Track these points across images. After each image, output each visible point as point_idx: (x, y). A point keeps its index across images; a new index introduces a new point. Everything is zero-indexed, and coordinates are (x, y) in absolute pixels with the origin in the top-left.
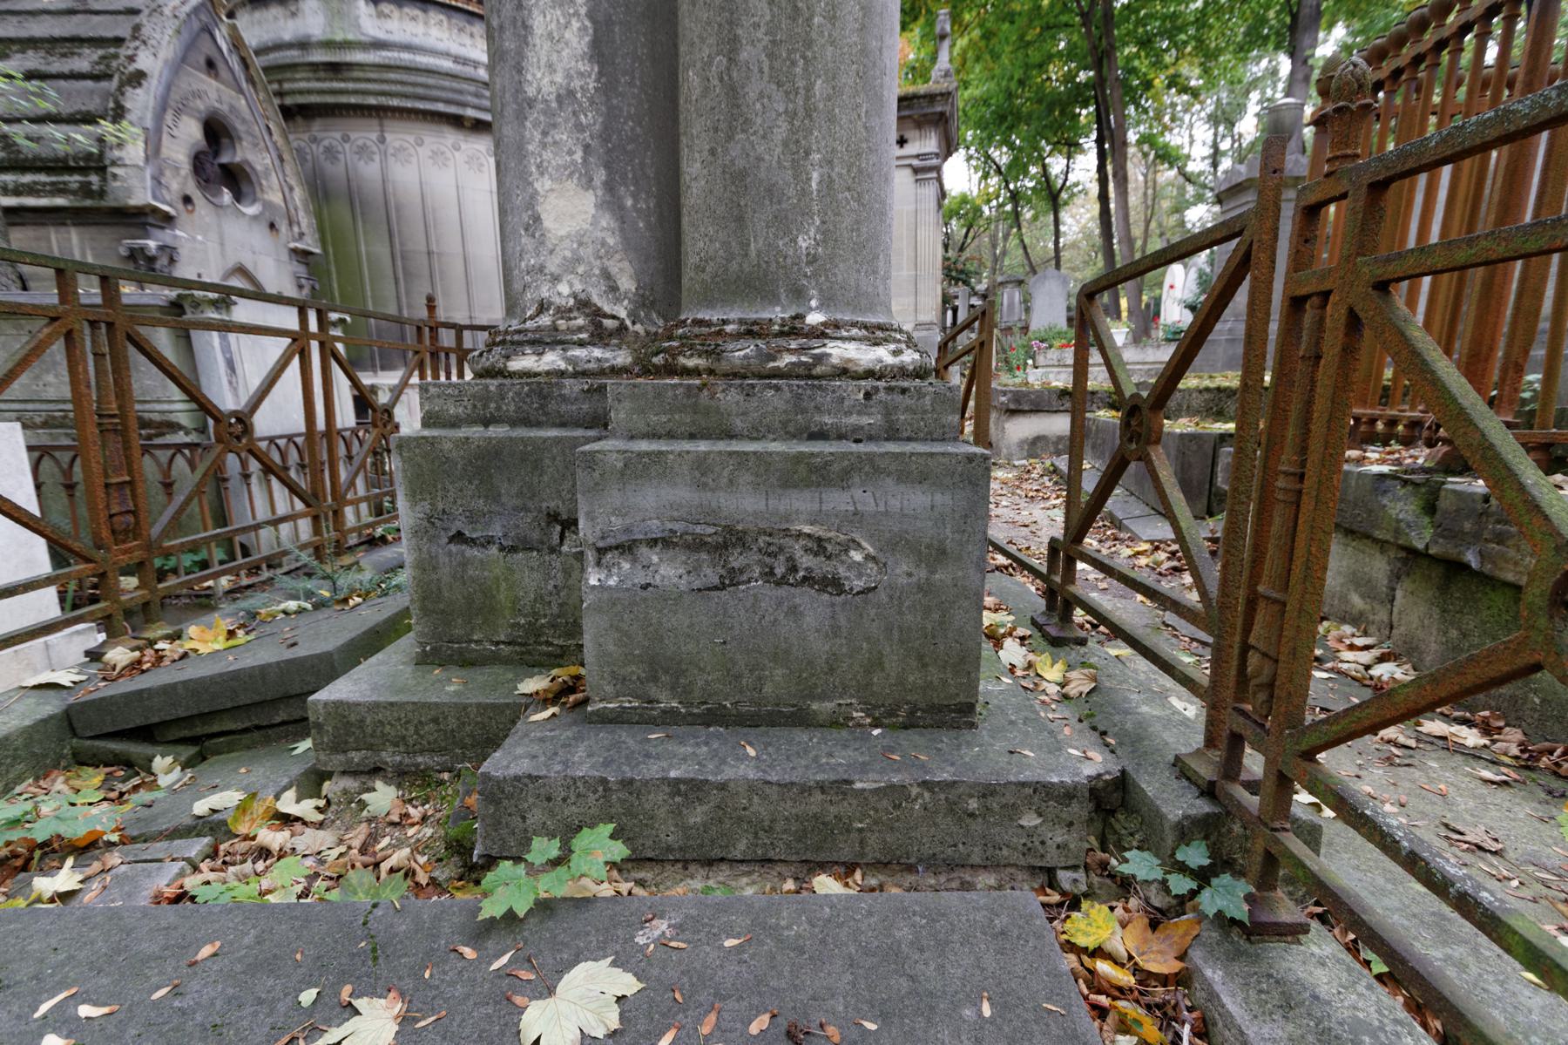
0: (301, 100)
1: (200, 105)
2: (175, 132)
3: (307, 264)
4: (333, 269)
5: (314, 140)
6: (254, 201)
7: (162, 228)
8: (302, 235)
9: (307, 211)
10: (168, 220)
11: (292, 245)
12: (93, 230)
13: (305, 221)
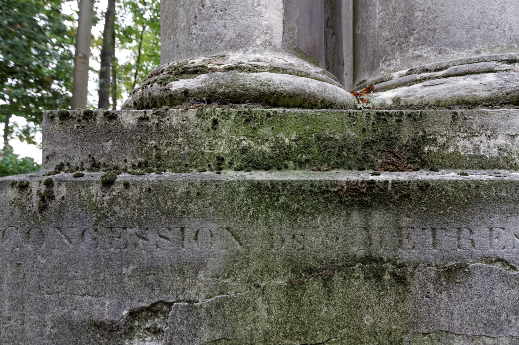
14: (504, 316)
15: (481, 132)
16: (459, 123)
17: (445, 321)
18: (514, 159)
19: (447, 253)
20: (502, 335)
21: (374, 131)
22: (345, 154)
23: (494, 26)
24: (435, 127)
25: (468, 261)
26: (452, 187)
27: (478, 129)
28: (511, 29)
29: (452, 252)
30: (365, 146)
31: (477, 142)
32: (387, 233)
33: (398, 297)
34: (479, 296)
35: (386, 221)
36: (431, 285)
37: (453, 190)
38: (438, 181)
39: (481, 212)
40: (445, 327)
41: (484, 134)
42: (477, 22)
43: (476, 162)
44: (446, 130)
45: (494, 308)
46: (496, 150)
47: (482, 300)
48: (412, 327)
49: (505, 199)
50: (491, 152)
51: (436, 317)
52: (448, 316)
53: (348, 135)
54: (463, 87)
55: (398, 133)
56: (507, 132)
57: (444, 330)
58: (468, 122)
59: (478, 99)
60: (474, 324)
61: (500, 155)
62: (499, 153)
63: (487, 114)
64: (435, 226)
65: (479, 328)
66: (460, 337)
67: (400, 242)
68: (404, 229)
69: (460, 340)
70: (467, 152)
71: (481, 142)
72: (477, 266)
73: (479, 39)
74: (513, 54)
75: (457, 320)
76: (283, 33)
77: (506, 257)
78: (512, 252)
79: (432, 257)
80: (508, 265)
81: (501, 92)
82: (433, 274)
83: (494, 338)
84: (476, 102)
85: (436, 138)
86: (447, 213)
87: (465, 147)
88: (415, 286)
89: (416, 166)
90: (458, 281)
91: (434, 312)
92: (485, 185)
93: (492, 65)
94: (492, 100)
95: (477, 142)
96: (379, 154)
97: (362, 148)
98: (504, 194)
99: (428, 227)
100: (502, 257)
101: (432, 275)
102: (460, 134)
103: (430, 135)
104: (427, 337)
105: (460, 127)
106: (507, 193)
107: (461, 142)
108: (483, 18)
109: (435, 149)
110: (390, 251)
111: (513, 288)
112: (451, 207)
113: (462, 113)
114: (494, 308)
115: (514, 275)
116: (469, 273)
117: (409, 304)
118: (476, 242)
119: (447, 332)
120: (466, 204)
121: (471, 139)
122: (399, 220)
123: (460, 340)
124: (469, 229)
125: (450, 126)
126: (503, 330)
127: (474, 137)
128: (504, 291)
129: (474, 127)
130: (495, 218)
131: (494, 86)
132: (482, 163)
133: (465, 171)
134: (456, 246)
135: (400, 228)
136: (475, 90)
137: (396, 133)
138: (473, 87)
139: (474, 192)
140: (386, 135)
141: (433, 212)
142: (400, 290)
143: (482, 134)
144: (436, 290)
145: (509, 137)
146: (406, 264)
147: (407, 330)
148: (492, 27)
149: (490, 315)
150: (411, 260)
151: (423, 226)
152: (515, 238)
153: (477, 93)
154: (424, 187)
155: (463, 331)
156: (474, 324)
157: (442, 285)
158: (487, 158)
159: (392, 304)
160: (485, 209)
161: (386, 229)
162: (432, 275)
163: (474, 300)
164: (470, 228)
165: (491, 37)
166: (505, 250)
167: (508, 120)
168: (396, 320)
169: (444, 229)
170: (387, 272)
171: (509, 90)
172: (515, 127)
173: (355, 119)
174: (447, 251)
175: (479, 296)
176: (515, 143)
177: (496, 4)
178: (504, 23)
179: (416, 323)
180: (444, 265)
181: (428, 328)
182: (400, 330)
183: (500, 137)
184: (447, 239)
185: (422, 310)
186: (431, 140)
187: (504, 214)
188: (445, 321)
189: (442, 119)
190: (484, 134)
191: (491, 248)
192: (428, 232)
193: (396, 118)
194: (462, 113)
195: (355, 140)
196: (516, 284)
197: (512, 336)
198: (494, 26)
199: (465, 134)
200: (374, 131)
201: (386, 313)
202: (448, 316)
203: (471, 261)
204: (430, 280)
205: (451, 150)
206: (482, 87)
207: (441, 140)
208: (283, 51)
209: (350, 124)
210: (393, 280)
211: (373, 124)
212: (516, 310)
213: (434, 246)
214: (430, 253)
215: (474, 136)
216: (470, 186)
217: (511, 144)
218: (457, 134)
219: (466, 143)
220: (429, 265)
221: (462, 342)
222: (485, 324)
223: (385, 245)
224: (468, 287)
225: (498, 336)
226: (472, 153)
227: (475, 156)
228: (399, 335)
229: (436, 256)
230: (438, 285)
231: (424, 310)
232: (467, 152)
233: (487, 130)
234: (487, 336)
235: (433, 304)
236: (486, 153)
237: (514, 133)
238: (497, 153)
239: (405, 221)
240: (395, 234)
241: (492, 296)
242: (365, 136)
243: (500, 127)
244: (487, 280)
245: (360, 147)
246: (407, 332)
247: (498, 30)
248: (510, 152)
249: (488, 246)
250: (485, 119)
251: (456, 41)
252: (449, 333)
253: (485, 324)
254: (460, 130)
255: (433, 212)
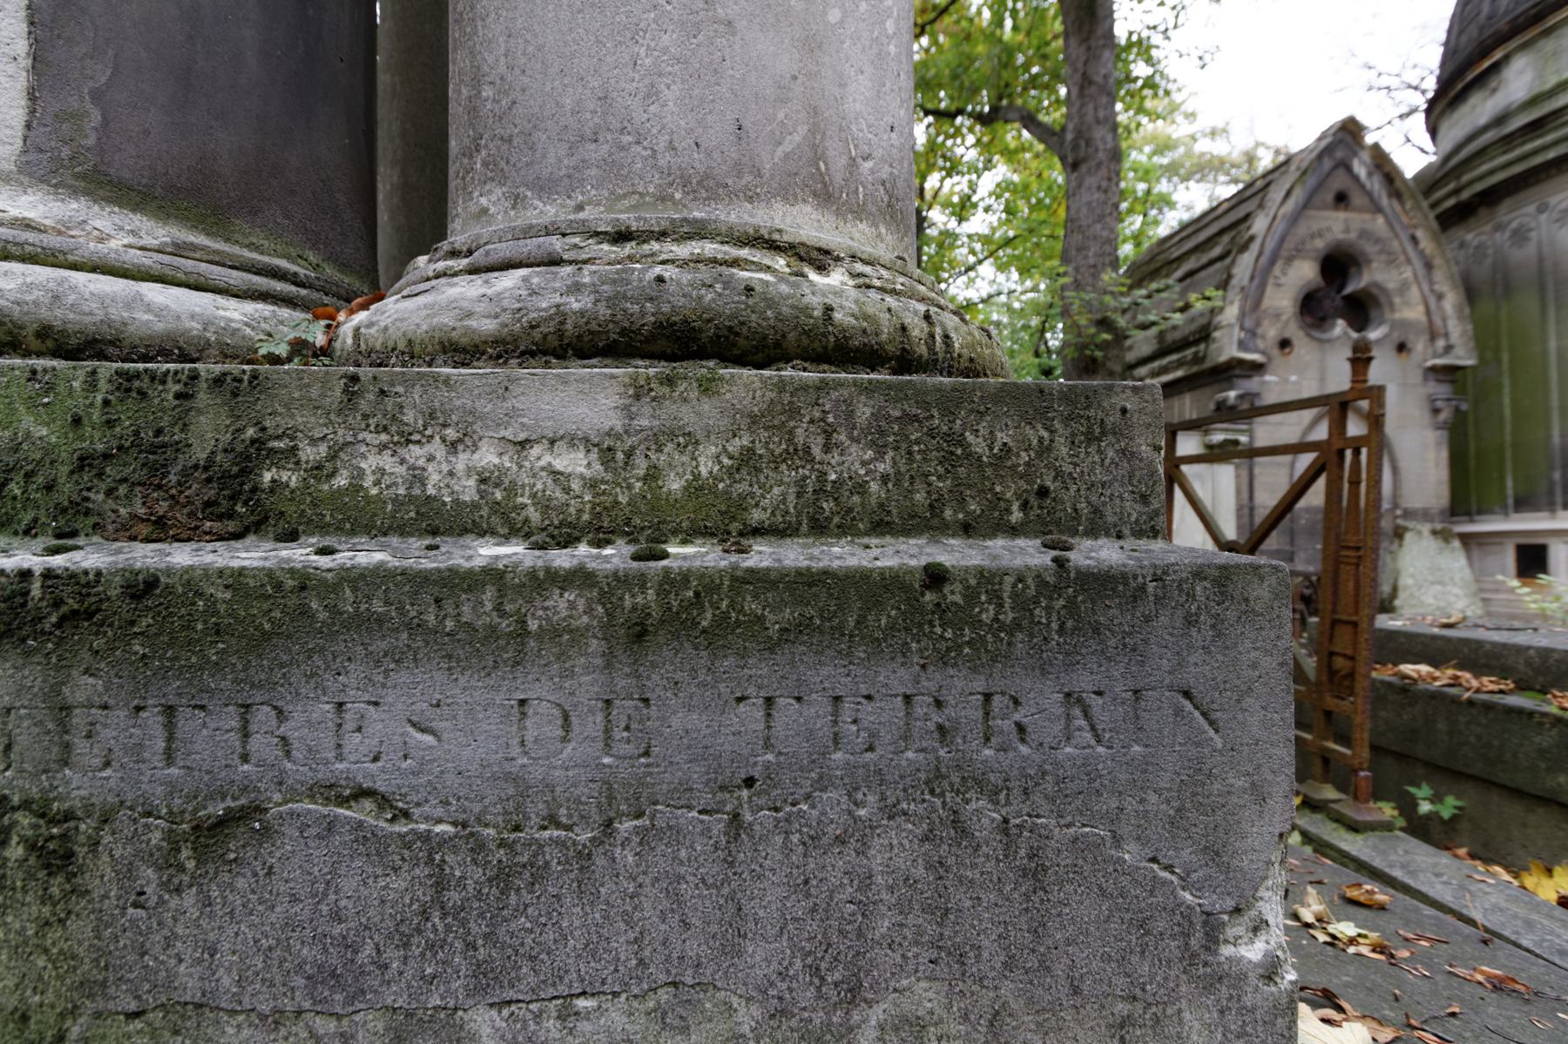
0: (1479, 187)
1: (1320, 244)
2: (1283, 280)
3: (1453, 382)
4: (1506, 381)
5: (1500, 227)
6: (1380, 324)
7: (1249, 377)
8: (1449, 349)
9: (1461, 318)
10: (1257, 368)
11: (1429, 363)
12: (1198, 392)
13: (1457, 330)
14: (369, 950)
15: (428, 432)
16: (363, 405)
17: (191, 975)
18: (524, 506)
19: (206, 778)
20: (362, 1006)
21: (110, 424)
22: (18, 492)
23: (630, 139)
24: (292, 416)
25: (269, 800)
26: (227, 587)
27: (420, 422)
28: (671, 147)
29: (223, 774)
30: (81, 468)
31: (417, 458)
32: (25, 724)
33: (46, 910)
34: (294, 899)
35: (20, 690)
36: (149, 871)
37: (228, 595)
38: (187, 572)
39: (310, 657)
40: (192, 992)
41: (437, 438)
42: (591, 124)
43: (412, 514)
44: (325, 425)
45: (337, 930)
46: (472, 482)
47: (302, 910)
48: (91, 996)
49: (380, 620)
50: (456, 488)
51: (162, 962)
52: (200, 961)
53: (28, 435)
54: (101, 299)
55: (182, 431)
56: (503, 433)
57: (188, 999)
58: (389, 403)
59: (477, 339)
60: (278, 979)
61: (482, 498)
62: (478, 491)
63: (447, 381)
64: (172, 700)
65: (293, 988)
66: (241, 1018)
67: (67, 746)
68: (77, 711)
69: (239, 1026)
70: (388, 487)
71: (431, 459)
72: (291, 813)
73: (594, 172)
74: (623, 216)
75: (229, 970)
76: (28, 126)
77: (381, 786)
78: (399, 769)
79: (159, 790)
80: (392, 807)
81: (519, 321)
82: (156, 837)
83: (339, 1017)
84: (476, 346)
85: (295, 449)
86: (208, 661)
87: (382, 471)
88: (100, 875)
89: (232, 526)
90: (232, 856)
91: (157, 949)
92: (323, 582)
93: (557, 244)
94: (504, 342)
95: (417, 458)
96: (122, 490)
97: (72, 472)
98: (378, 607)
99: (151, 702)
100: (370, 784)
101: (154, 842)
102: (369, 437)
103: (278, 438)
104: (138, 1024)
105: (365, 417)
106: (387, 603)
107: (371, 458)
108: (605, 113)
109: (294, 478)
110: (35, 775)
111: (395, 870)
112: (221, 646)
113: (375, 378)
114: (337, 930)
115: (399, 835)
116: (267, 832)
117: (81, 928)
118: (296, 745)
119: (199, 1006)
120: (266, 636)
121: (402, 451)
122: (64, 683)
123: (239, 1026)
124: (275, 708)
125: (340, 412)
126: (363, 992)
127: (411, 446)
128: (370, 881)
129: (409, 416)
130: (353, 675)
131: (505, 303)
132: (435, 520)
133: (328, 541)
134: (235, 756)
135: (66, 709)
136: (470, 315)
137: (176, 430)
138: (465, 304)
139: (292, 601)
140: (147, 435)
141: (169, 659)
142: (55, 891)
143: (432, 437)
144: (164, 885)
145: (511, 447)
146: (79, 813)
147: (75, 1007)
148: (627, 139)
149: (325, 950)
150: (93, 800)
151: (136, 702)
152: (411, 730)
153: (473, 323)
154: (143, 587)
155: (246, 1000)
156: (278, 979)
157: (182, 869)
158: (444, 504)
159: (30, 932)
160: (322, 650)
161: (23, 711)
162: (154, 842)
163: (278, 909)
164: (279, 704)
165: (622, 167)
166: (379, 764)
167: (504, 399)
168: (40, 978)
169: (202, 707)
170: (15, 839)
171: (535, 315)
172: (525, 420)
173: (49, 388)
174: (208, 772)
175: (294, 899)
176: (527, 464)
177: (637, 77)
178: (654, 131)
179: (104, 984)
180: (196, 811)
181: (138, 997)
182: (53, 1007)
183: (484, 446)
184: (209, 737)
185: (121, 944)
186: (282, 451)
187: (378, 664)
188: (191, 975)
189: (314, 392)
190: (437, 438)
191: (340, 758)
192: (153, 719)
193: (177, 387)
194: (375, 378)
195: (48, 450)
196: (403, 859)
197: (395, 1009)
198: (630, 139)
199: (384, 437)
200: (110, 424)
201: (10, 959)
202: (200, 961)
203: (277, 797)
204: (148, 857)
205: (341, 481)
206: (480, 308)
207: (310, 453)
208: (26, 180)
209: (32, 404)
210: (32, 861)
211: (106, 403)
212: (402, 934)
213: (169, 757)
214: (156, 779)
215: (409, 441)
216: (278, 586)
217: (515, 467)
218: (360, 437)
219: (387, 461)
220: (149, 814)
221: (246, 1033)
222: (309, 978)
223: (18, 758)
224: (261, 873)
225: (351, 1009)
226: (402, 491)
227: (411, 498)
228: (52, 1021)
229: (172, 788)
230: (172, 871)
231: (125, 946)
232: (388, 487)
233: (445, 426)
234: (318, 1013)
235: (155, 925)
236: (444, 491)
237: (522, 436)
238: (474, 491)
239: (82, 688)
240: (51, 726)
241: (332, 897)
242: (82, 438)
243: (483, 417)
244: (318, 851)
245: (65, 469)
246: (74, 1012)
247: (639, 149)
248: (511, 491)
249: (331, 755)
250: (440, 396)
251: (545, 173)
252: (207, 1011)
253: (309, 978)
254: (368, 426)
255: (169, 659)
